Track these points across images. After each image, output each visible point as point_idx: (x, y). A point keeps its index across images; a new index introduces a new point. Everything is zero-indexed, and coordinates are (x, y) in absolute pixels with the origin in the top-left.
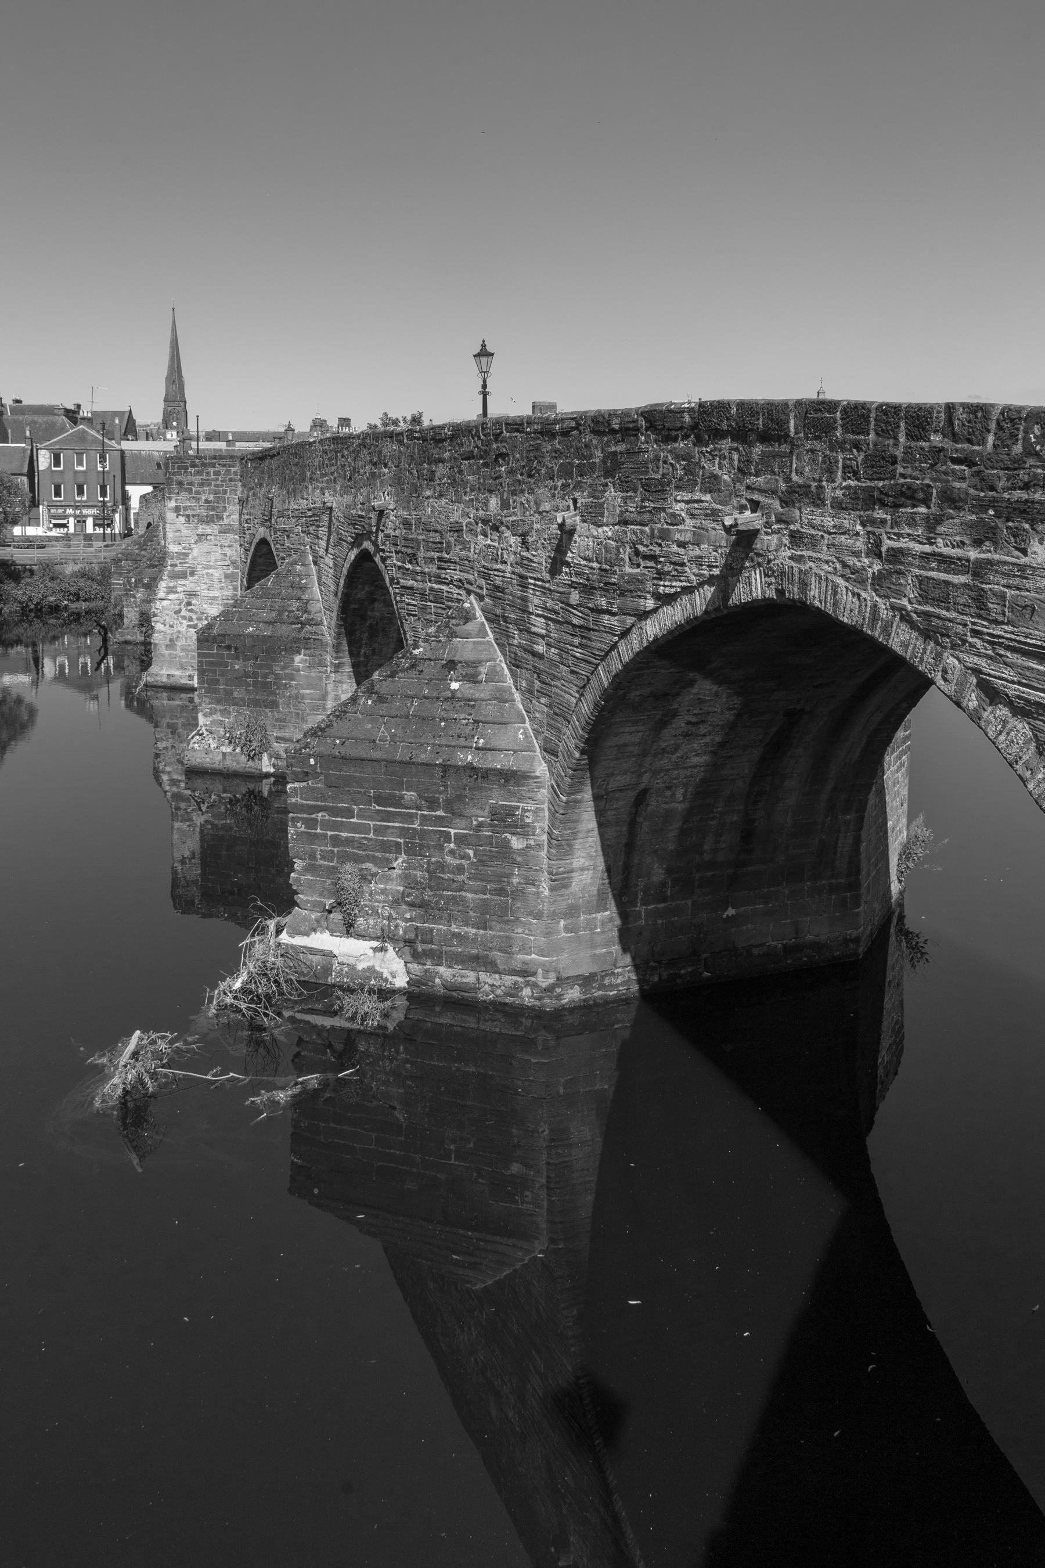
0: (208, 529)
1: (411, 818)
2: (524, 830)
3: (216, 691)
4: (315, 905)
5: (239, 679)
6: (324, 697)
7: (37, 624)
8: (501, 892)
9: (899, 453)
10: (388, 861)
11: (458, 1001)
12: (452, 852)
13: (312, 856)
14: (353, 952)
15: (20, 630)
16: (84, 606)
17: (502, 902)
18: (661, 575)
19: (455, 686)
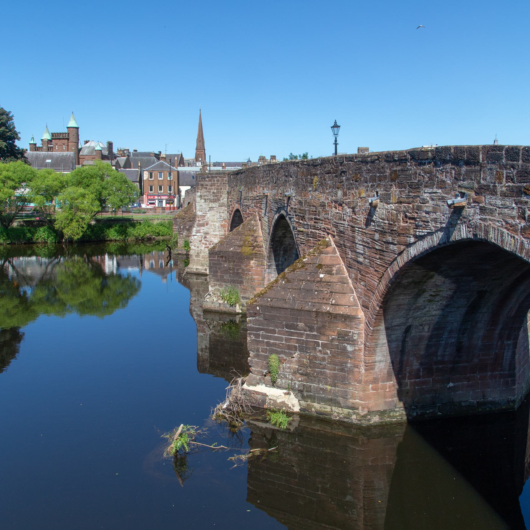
0: (214, 205)
1: (301, 335)
2: (353, 342)
3: (216, 276)
5: (227, 271)
6: (263, 279)
7: (142, 246)
8: (342, 370)
10: (291, 354)
11: (323, 419)
12: (320, 351)
13: (258, 350)
16: (161, 238)
17: (343, 375)
18: (417, 227)
19: (322, 276)
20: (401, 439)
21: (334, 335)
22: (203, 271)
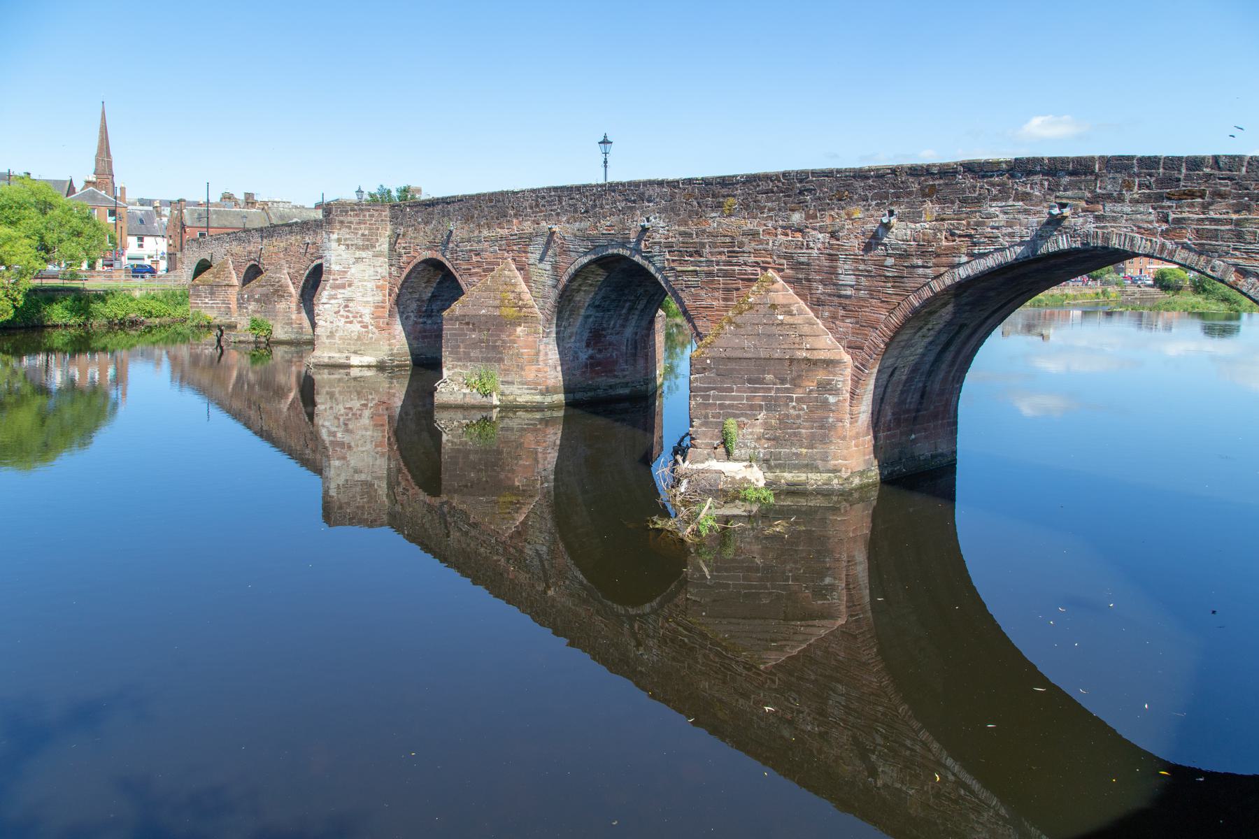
0: (363, 254)
1: (770, 390)
2: (836, 392)
3: (457, 353)
4: (707, 445)
5: (475, 344)
6: (537, 354)
7: (121, 335)
8: (822, 427)
9: (1182, 177)
11: (794, 491)
12: (794, 407)
13: (706, 417)
14: (734, 470)
15: (105, 340)
16: (157, 321)
17: (823, 431)
18: (975, 244)
19: (780, 317)
20: (875, 503)
21: (812, 385)
22: (342, 361)
